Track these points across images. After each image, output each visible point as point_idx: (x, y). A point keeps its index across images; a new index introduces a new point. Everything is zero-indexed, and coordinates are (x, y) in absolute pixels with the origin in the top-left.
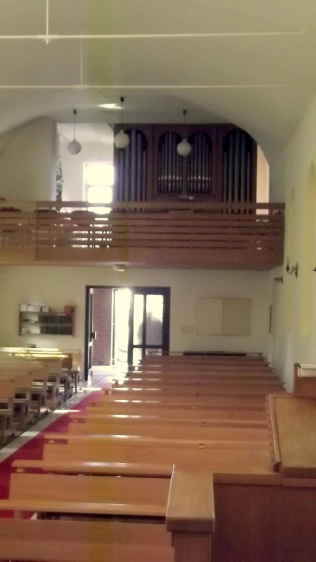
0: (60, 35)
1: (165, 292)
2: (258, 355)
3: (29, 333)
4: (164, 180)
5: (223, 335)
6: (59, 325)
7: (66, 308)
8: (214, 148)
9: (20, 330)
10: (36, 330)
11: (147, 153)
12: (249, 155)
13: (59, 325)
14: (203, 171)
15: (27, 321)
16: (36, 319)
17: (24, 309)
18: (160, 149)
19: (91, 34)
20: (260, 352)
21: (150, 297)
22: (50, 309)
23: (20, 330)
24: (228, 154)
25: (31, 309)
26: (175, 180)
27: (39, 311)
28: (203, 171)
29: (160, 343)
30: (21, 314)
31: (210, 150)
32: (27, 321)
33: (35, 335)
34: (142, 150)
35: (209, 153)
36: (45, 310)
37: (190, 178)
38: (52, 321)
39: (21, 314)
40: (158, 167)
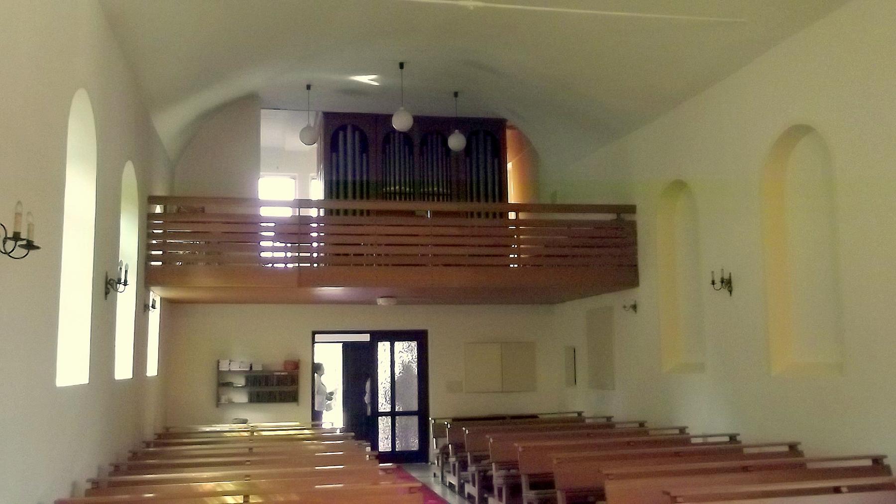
0: (486, 2)
1: (420, 337)
2: (576, 415)
3: (231, 403)
5: (502, 392)
6: (276, 389)
7: (286, 363)
8: (372, 149)
9: (218, 400)
10: (241, 398)
11: (368, 157)
12: (364, 157)
13: (276, 389)
14: (440, 184)
15: (229, 385)
16: (240, 381)
17: (224, 367)
18: (384, 152)
19: (535, 11)
20: (608, 415)
21: (398, 345)
22: (263, 366)
23: (218, 400)
24: (338, 157)
25: (235, 367)
26: (389, 192)
27: (248, 369)
28: (440, 184)
29: (415, 407)
30: (220, 373)
31: (411, 153)
32: (229, 385)
33: (240, 405)
34: (361, 153)
35: (446, 159)
36: (257, 368)
37: (424, 189)
38: (267, 385)
39: (220, 373)
40: (414, 177)
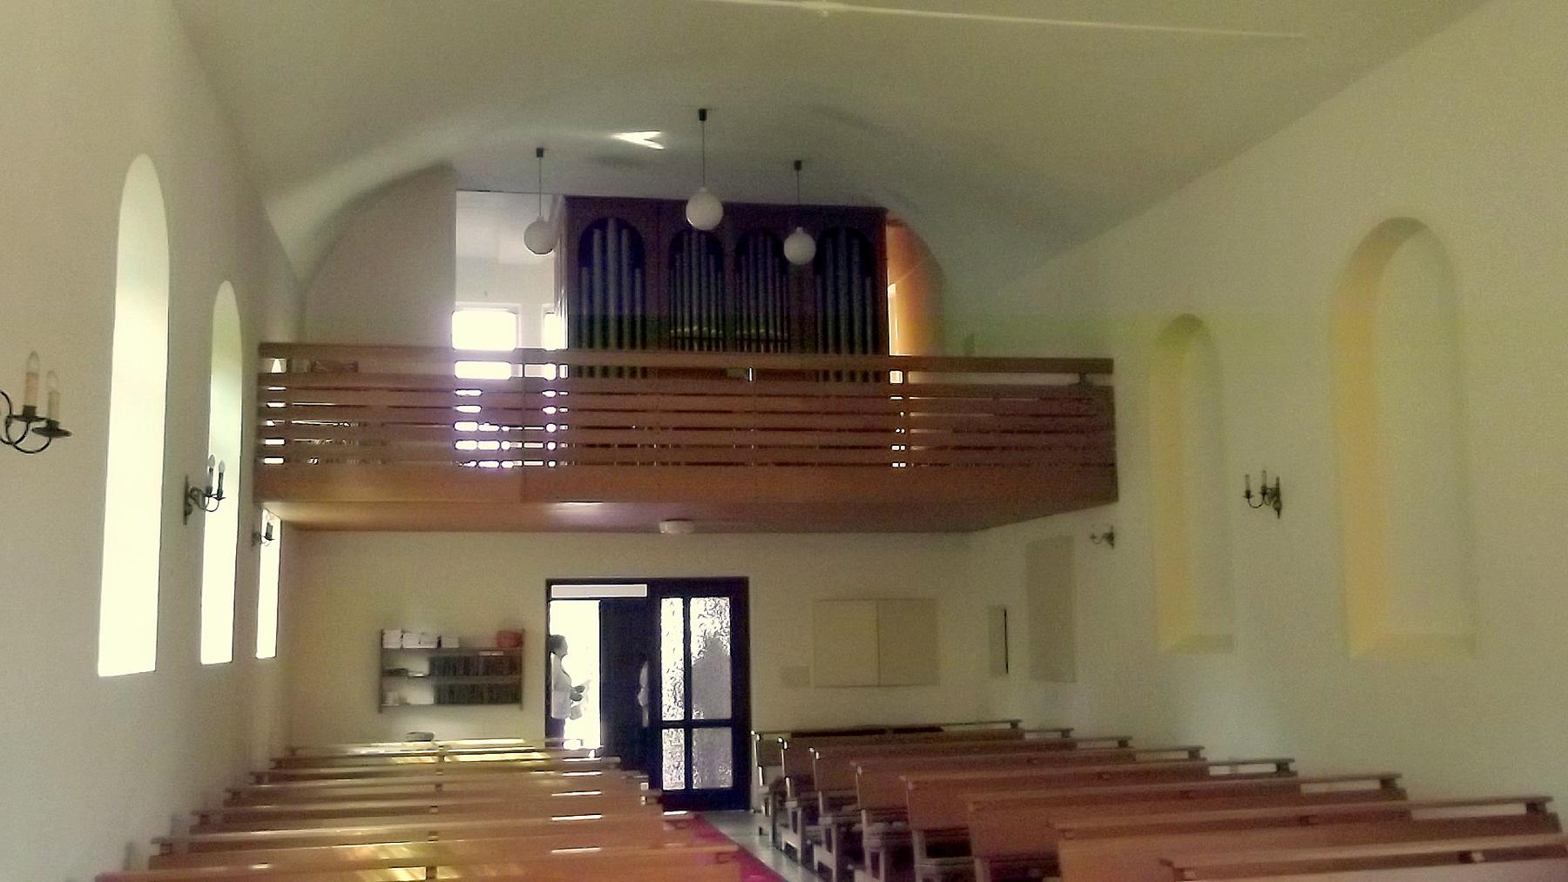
0: (850, 4)
1: (734, 590)
2: (1008, 726)
3: (404, 705)
4: (750, 336)
5: (879, 686)
6: (482, 681)
7: (501, 636)
8: (650, 261)
9: (382, 699)
10: (422, 696)
11: (643, 274)
12: (638, 275)
13: (482, 681)
14: (771, 321)
15: (400, 673)
16: (421, 668)
17: (392, 642)
18: (672, 265)
19: (937, 20)
20: (1064, 726)
21: (697, 604)
22: (460, 640)
23: (382, 699)
24: (591, 274)
25: (411, 643)
26: (681, 336)
27: (433, 646)
28: (771, 321)
29: (726, 712)
30: (384, 653)
31: (720, 267)
32: (400, 673)
33: (421, 709)
34: (632, 268)
35: (781, 278)
36: (450, 643)
37: (742, 330)
38: (467, 673)
39: (384, 653)
40: (724, 310)
